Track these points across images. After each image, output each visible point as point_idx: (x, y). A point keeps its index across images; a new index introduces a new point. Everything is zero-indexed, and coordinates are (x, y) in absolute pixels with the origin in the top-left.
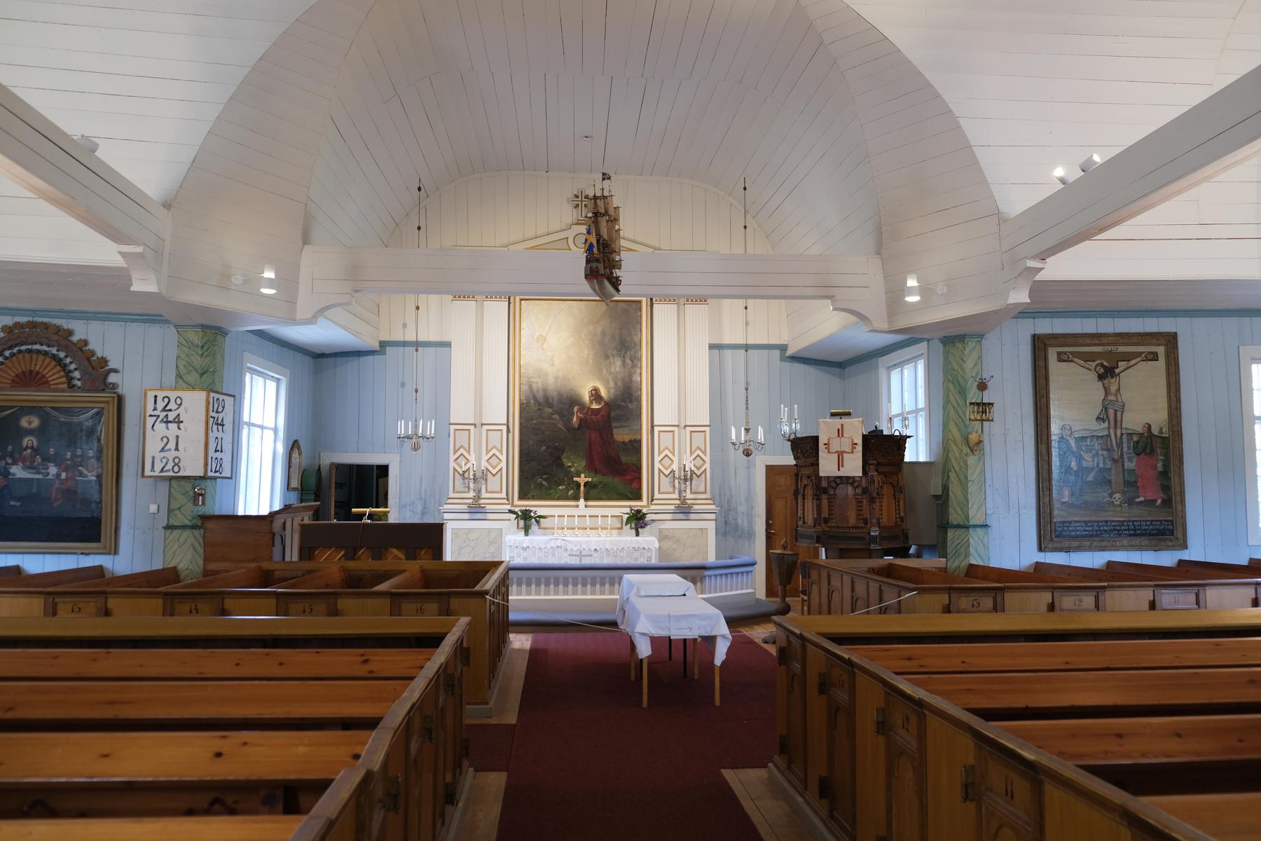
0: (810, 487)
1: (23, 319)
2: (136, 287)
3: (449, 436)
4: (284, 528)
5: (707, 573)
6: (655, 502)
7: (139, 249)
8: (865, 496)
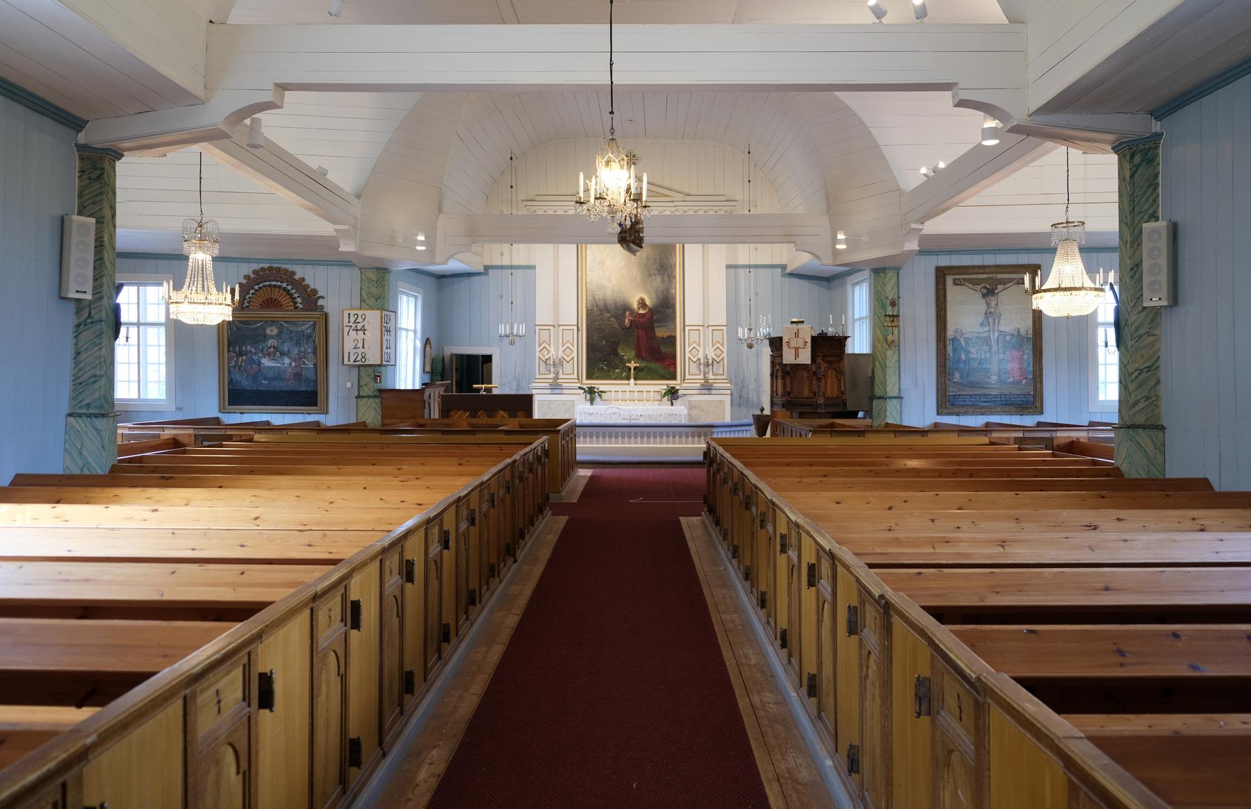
0: (780, 370)
1: (266, 266)
2: (342, 249)
3: (535, 333)
4: (430, 398)
5: (715, 430)
6: (686, 381)
7: (346, 227)
8: (814, 377)
